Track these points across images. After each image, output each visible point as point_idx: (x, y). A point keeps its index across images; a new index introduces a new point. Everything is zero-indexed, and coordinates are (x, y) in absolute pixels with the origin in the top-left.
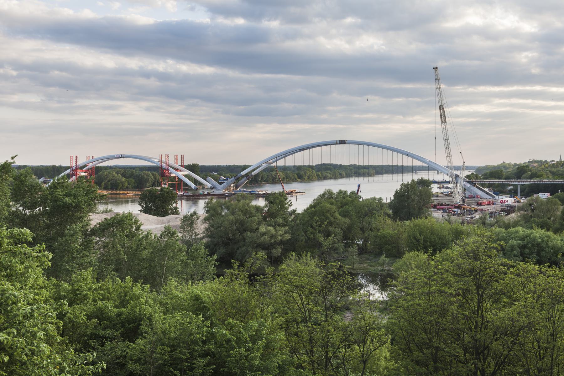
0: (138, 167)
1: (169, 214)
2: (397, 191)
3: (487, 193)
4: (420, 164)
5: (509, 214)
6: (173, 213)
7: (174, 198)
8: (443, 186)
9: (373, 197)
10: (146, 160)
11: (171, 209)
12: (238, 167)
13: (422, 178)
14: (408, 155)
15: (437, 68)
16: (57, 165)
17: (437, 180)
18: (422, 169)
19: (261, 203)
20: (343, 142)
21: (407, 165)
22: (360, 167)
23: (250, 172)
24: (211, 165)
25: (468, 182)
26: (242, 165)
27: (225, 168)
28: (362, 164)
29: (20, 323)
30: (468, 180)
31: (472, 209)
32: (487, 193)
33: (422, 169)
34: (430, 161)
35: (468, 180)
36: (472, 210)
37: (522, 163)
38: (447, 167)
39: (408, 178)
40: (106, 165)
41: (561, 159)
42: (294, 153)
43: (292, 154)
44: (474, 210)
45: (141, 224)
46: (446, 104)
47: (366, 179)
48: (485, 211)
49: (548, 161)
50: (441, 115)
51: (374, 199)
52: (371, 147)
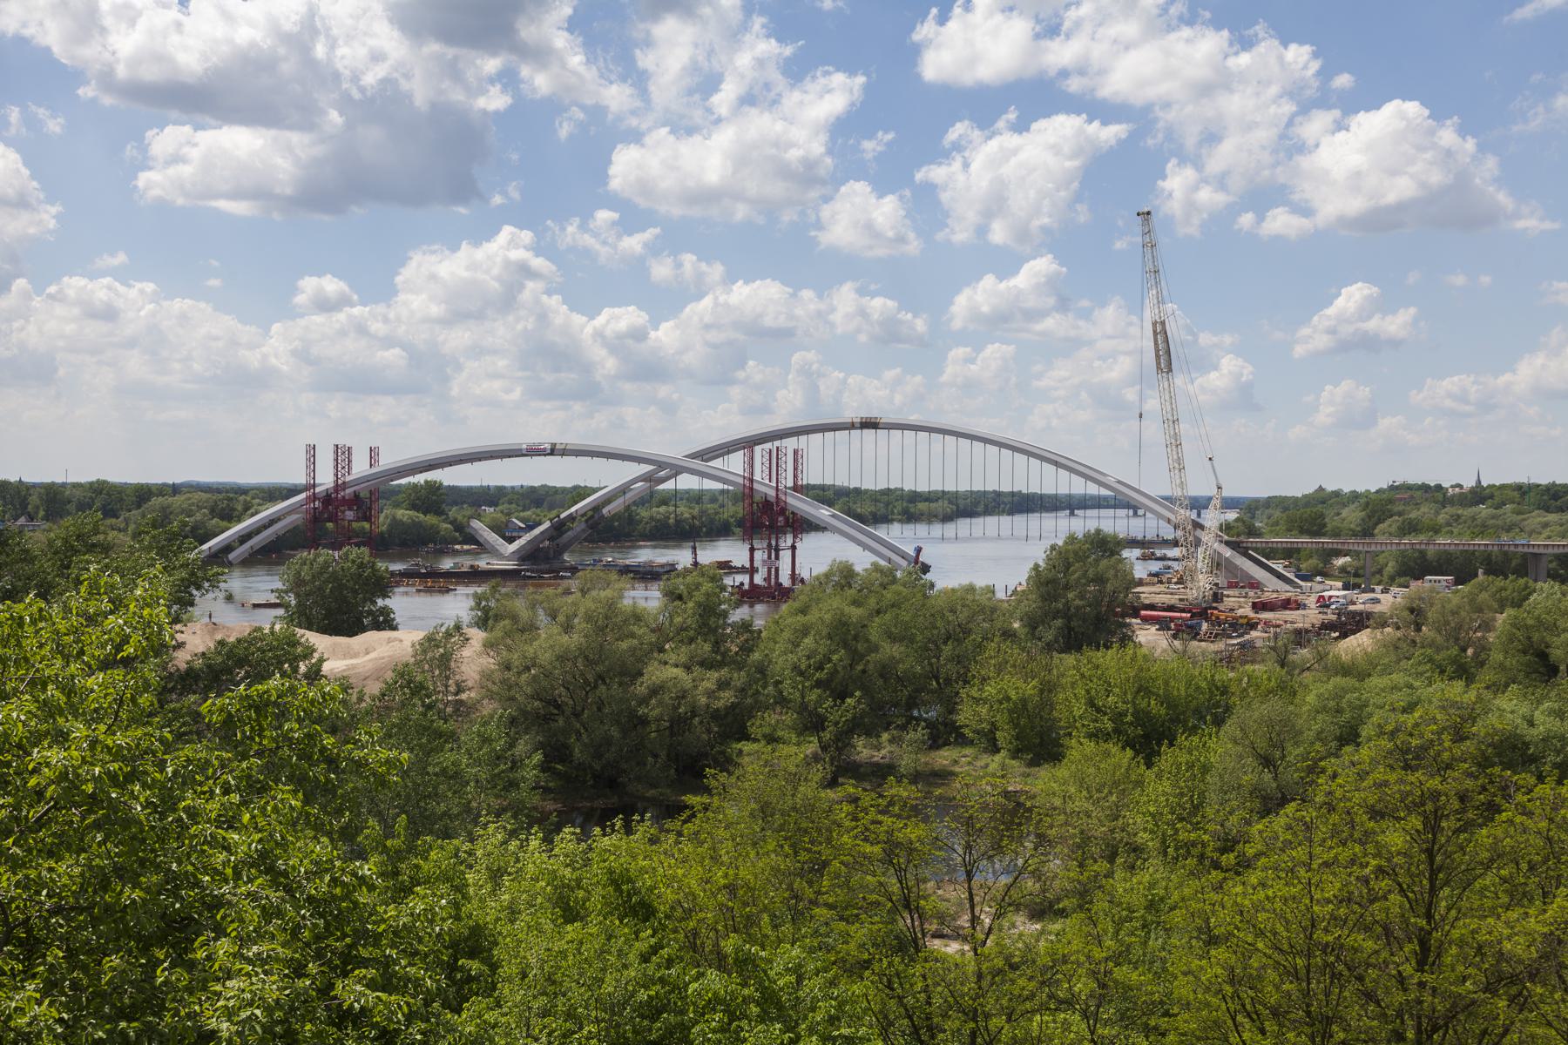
0: (257, 489)
1: (363, 630)
2: (1036, 566)
3: (1279, 576)
4: (1093, 489)
5: (1344, 635)
6: (378, 627)
7: (383, 586)
8: (1153, 554)
9: (965, 582)
10: (1087, 478)
11: (370, 613)
12: (242, 491)
13: (1098, 531)
14: (1056, 464)
15: (1148, 213)
16: (12, 480)
17: (1140, 537)
18: (1098, 503)
19: (648, 599)
20: (870, 424)
21: (940, 489)
22: (915, 497)
23: (596, 508)
24: (477, 484)
25: (1227, 543)
26: (569, 485)
27: (518, 493)
28: (922, 487)
29: (796, 897)
30: (1226, 538)
31: (1241, 621)
32: (1279, 576)
33: (1098, 503)
34: (1119, 482)
35: (1226, 538)
36: (1242, 625)
37: (1373, 490)
38: (1166, 498)
39: (1057, 529)
40: (475, 483)
41: (1479, 481)
42: (729, 453)
43: (722, 455)
44: (1248, 624)
45: (321, 661)
46: (1171, 318)
47: (937, 529)
48: (1278, 626)
49: (1445, 485)
50: (1157, 351)
51: (971, 589)
52: (923, 435)
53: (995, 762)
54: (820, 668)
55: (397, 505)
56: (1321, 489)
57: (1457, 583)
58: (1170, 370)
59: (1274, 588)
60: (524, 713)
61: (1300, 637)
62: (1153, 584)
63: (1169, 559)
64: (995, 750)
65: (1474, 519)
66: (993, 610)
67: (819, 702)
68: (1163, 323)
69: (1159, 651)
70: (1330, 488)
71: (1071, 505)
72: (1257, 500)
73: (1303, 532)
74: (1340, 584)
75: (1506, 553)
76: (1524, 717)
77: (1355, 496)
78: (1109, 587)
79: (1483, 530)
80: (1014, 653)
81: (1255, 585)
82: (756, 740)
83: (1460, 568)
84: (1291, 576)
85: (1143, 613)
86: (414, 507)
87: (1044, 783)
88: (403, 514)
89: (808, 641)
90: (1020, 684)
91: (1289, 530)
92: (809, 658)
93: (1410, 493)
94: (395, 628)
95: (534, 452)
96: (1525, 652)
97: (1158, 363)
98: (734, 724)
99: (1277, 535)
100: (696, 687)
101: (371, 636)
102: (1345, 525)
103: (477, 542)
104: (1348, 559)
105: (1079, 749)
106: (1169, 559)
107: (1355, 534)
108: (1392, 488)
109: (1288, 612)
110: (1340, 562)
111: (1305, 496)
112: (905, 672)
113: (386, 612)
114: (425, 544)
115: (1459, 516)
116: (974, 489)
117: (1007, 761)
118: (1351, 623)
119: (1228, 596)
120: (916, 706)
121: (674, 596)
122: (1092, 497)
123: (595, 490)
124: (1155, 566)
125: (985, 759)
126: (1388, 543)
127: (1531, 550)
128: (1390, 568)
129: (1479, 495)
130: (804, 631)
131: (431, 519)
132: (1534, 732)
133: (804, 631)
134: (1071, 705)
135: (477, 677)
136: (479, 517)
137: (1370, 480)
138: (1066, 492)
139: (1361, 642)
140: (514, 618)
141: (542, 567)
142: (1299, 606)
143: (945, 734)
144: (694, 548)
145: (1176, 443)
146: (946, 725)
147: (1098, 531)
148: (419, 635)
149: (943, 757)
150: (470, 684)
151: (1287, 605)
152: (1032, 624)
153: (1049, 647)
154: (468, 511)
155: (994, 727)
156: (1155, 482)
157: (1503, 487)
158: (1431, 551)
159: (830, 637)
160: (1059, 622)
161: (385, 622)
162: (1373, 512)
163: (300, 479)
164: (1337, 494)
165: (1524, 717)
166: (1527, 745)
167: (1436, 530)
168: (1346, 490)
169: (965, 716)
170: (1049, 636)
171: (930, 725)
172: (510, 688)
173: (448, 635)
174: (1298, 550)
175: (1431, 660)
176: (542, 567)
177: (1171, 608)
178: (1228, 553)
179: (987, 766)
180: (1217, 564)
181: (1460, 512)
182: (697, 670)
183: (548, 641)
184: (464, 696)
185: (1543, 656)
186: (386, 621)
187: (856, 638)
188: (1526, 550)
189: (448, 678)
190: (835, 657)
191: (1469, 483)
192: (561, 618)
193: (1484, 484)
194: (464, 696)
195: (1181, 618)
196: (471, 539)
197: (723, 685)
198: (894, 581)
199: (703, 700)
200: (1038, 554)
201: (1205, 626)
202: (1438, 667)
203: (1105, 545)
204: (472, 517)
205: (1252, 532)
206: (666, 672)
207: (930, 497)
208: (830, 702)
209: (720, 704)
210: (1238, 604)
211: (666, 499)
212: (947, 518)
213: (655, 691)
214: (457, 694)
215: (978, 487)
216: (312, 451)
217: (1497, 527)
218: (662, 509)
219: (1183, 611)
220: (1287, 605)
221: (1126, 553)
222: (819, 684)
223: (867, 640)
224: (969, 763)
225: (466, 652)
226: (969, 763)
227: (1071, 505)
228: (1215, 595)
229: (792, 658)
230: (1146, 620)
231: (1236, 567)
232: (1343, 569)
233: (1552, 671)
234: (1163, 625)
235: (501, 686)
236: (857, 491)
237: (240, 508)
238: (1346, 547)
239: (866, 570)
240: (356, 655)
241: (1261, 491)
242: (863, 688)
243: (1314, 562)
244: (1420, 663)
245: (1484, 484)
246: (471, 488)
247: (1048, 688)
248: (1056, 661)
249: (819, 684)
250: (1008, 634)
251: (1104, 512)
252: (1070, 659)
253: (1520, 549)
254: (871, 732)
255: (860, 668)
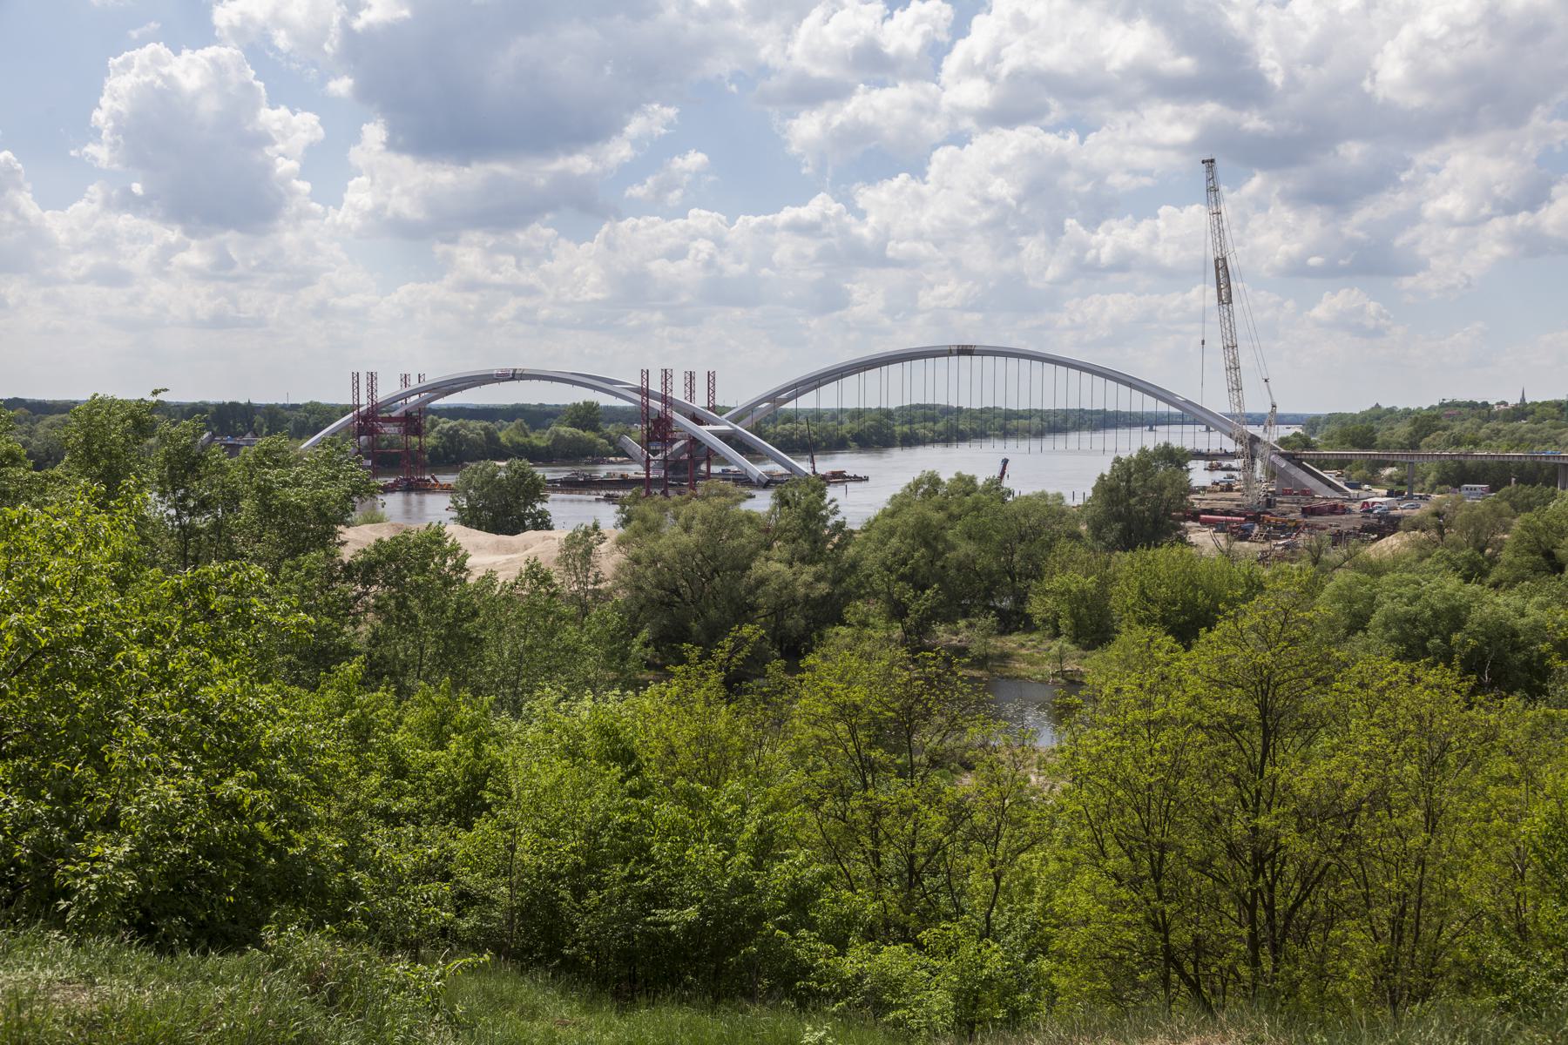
1: (525, 529)
2: (1102, 476)
4: (1163, 407)
6: (536, 527)
7: (535, 490)
8: (1220, 465)
9: (1038, 490)
10: (1158, 397)
11: (531, 515)
13: (1167, 445)
14: (1131, 385)
15: (1212, 161)
17: (1204, 450)
22: (1010, 415)
25: (1283, 455)
32: (1330, 485)
34: (1187, 401)
35: (1282, 450)
39: (1130, 443)
41: (1523, 399)
42: (842, 377)
43: (836, 379)
45: (466, 556)
47: (1024, 445)
51: (1043, 496)
53: (1055, 646)
54: (904, 563)
55: (560, 424)
56: (1377, 406)
57: (1492, 491)
58: (1230, 302)
59: (1323, 494)
60: (651, 601)
61: (1338, 538)
62: (1216, 492)
63: (1234, 470)
64: (1057, 634)
65: (1513, 433)
66: (1063, 513)
67: (902, 594)
68: (1224, 260)
69: (1207, 550)
70: (1385, 405)
71: (1150, 421)
72: (1318, 417)
73: (1355, 445)
74: (1385, 492)
75: (1538, 464)
76: (1516, 610)
77: (1408, 412)
78: (1167, 494)
79: (1519, 442)
80: (1081, 553)
81: (1307, 493)
82: (850, 625)
83: (1494, 476)
84: (1341, 484)
85: (1203, 516)
86: (573, 425)
87: (1094, 667)
88: (566, 431)
89: (894, 541)
90: (1080, 578)
91: (1343, 443)
92: (894, 555)
93: (1458, 409)
94: (550, 528)
95: (514, 376)
96: (1533, 553)
97: (1220, 299)
98: (828, 612)
99: (1332, 448)
100: (796, 580)
101: (530, 535)
102: (1394, 438)
103: (628, 456)
104: (1395, 469)
105: (1131, 637)
106: (1234, 470)
107: (1402, 447)
108: (1442, 405)
109: (1334, 517)
110: (1388, 471)
111: (1362, 413)
112: (983, 568)
113: (543, 514)
114: (584, 456)
115: (1499, 431)
116: (1033, 407)
117: (1066, 645)
118: (1386, 525)
119: (1282, 502)
120: (992, 597)
121: (783, 501)
122: (1162, 414)
123: (730, 409)
124: (1220, 476)
125: (1048, 643)
126: (1436, 453)
127: (1561, 461)
128: (1431, 478)
129: (1522, 411)
130: (892, 533)
131: (589, 435)
132: (1524, 621)
133: (892, 533)
134: (1123, 597)
135: (614, 569)
136: (629, 433)
137: (1424, 400)
138: (1027, 407)
139: (1392, 544)
140: (644, 519)
141: (682, 476)
142: (1345, 511)
143: (1014, 621)
144: (813, 461)
145: (1234, 367)
146: (1018, 613)
147: (1167, 445)
148: (564, 535)
149: (1011, 642)
150: (608, 576)
151: (1334, 510)
152: (1097, 529)
153: (1111, 548)
154: (622, 427)
155: (1057, 617)
156: (1218, 402)
157: (1544, 404)
158: (1469, 461)
159: (913, 537)
160: (1119, 526)
161: (543, 523)
162: (1421, 427)
163: (346, 399)
164: (1391, 411)
165: (1516, 610)
166: (1515, 634)
167: (1476, 443)
168: (1400, 407)
169: (1036, 607)
170: (1111, 538)
171: (1000, 612)
172: (639, 578)
173: (586, 534)
174: (1350, 462)
175: (1448, 559)
176: (682, 476)
177: (1227, 513)
178: (1283, 464)
179: (1050, 648)
180: (1272, 473)
181: (1500, 427)
182: (797, 565)
183: (674, 537)
184: (602, 586)
185: (1549, 555)
186: (543, 522)
187: (935, 538)
188: (1556, 461)
189: (588, 570)
190: (917, 555)
191: (1514, 400)
192: (682, 519)
193: (1528, 401)
194: (602, 586)
195: (1236, 522)
196: (622, 453)
197: (819, 578)
198: (975, 489)
199: (802, 591)
200: (1105, 467)
201: (1256, 529)
202: (1454, 565)
203: (1175, 458)
204: (623, 433)
205: (1307, 445)
206: (773, 567)
207: (1029, 414)
208: (912, 593)
209: (815, 594)
210: (1289, 509)
211: (792, 417)
212: (1040, 434)
213: (762, 582)
214: (596, 583)
215: (1061, 406)
216: (356, 377)
217: (1533, 441)
218: (788, 426)
219: (1238, 515)
220: (1334, 510)
221: (1191, 464)
222: (902, 577)
223: (946, 541)
224: (1035, 647)
225: (603, 548)
226: (1035, 647)
227: (1150, 421)
228: (1269, 501)
229: (880, 555)
230: (1205, 523)
231: (1290, 476)
232: (1390, 479)
233: (1561, 569)
234: (1220, 527)
235: (632, 575)
236: (959, 410)
237: (428, 425)
238: (1391, 459)
239: (951, 480)
240: (515, 551)
241: (1323, 410)
242: (941, 580)
243: (1363, 472)
244: (1438, 562)
245: (1528, 401)
246: (195, 404)
247: (1105, 583)
248: (1114, 559)
249: (902, 577)
250: (1076, 537)
251: (1173, 428)
252: (1127, 556)
253: (1551, 460)
254: (949, 619)
255: (939, 563)
